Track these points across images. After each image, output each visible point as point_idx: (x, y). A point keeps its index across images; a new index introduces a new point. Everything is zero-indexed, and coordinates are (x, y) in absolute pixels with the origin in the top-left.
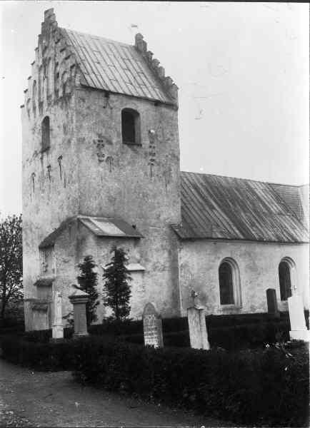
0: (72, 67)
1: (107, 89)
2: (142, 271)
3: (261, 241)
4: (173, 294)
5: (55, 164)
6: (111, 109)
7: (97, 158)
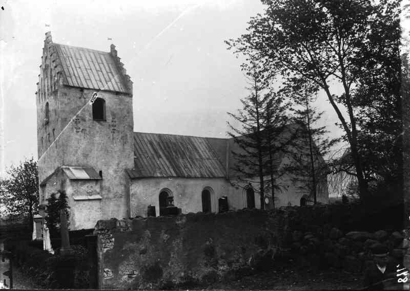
0: (58, 73)
1: (81, 86)
2: (100, 200)
3: (189, 177)
4: (127, 211)
5: (51, 132)
6: (85, 98)
7: (75, 130)
